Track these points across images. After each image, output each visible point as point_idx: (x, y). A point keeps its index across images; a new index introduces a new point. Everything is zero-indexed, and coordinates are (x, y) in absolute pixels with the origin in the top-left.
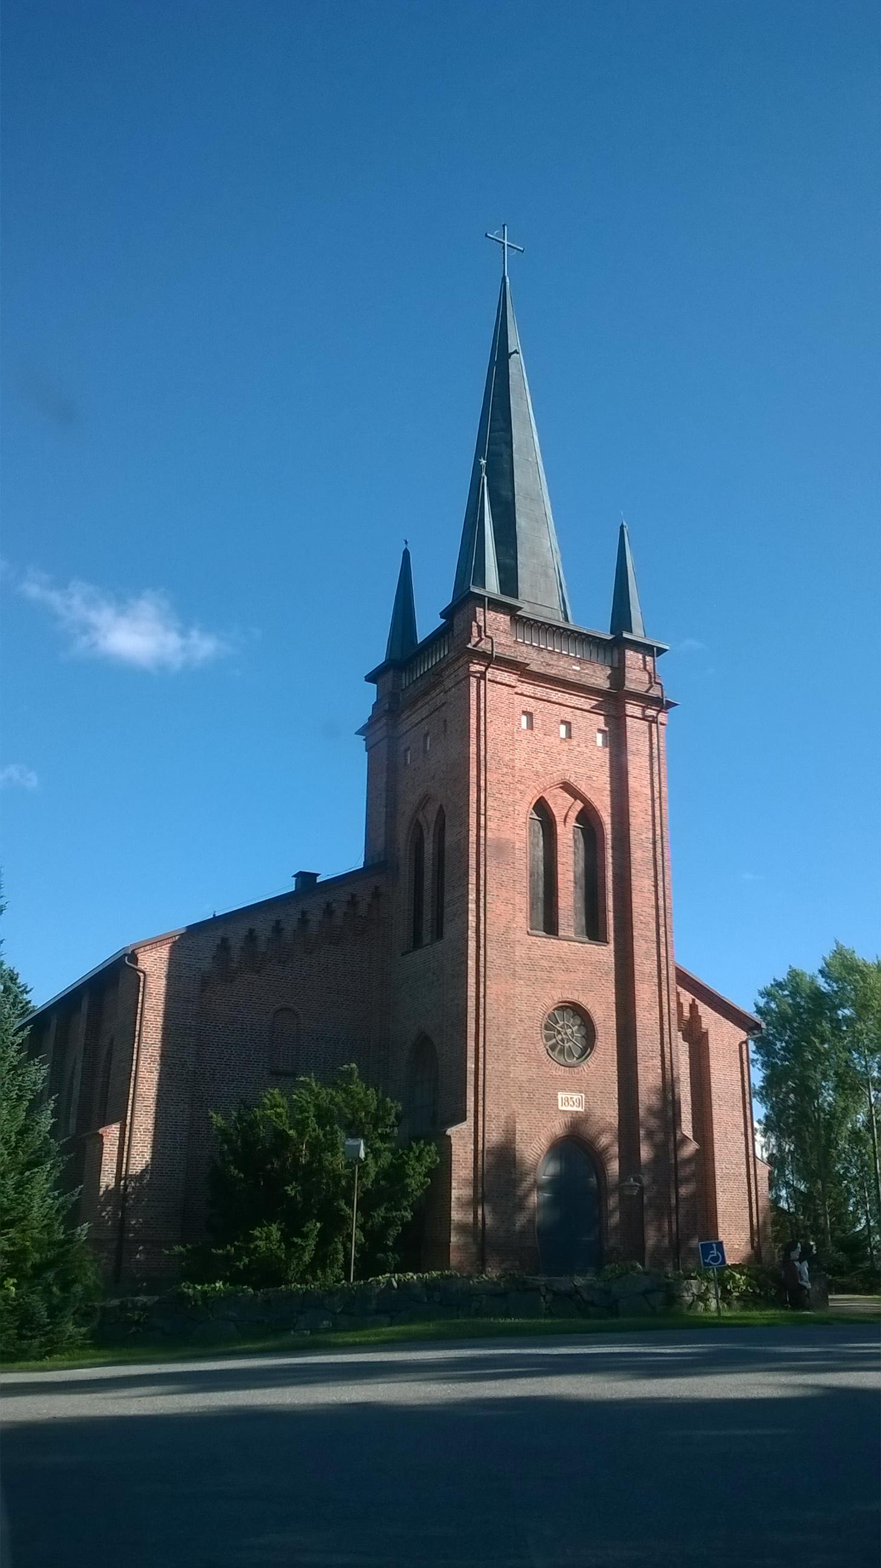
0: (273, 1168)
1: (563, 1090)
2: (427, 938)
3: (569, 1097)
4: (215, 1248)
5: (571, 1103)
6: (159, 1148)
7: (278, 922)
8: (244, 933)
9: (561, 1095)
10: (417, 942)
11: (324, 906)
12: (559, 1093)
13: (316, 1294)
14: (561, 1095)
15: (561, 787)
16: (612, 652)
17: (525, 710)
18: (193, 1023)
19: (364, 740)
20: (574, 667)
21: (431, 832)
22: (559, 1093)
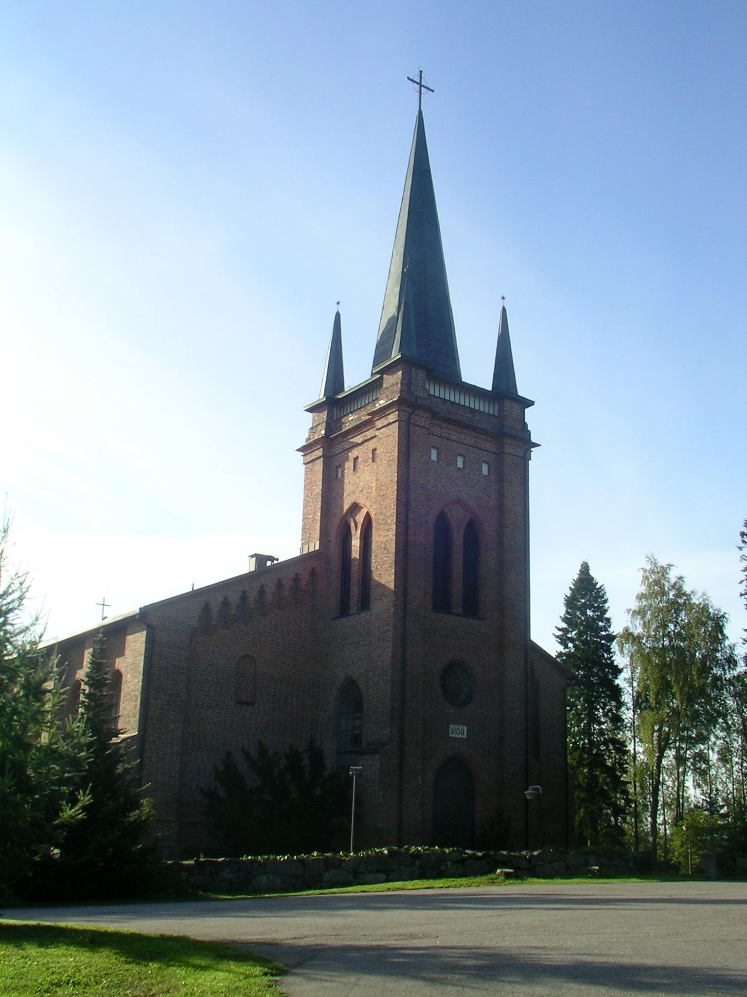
0: (87, 703)
1: (453, 723)
2: (354, 610)
3: (457, 728)
4: (92, 786)
5: (458, 732)
6: (162, 754)
7: (244, 592)
8: (220, 599)
9: (451, 726)
10: (344, 610)
11: (276, 581)
12: (450, 725)
13: (611, 987)
14: (451, 726)
15: (340, 409)
16: (494, 404)
17: (433, 446)
18: (185, 665)
19: (302, 456)
20: (468, 415)
21: (359, 532)
22: (450, 725)
